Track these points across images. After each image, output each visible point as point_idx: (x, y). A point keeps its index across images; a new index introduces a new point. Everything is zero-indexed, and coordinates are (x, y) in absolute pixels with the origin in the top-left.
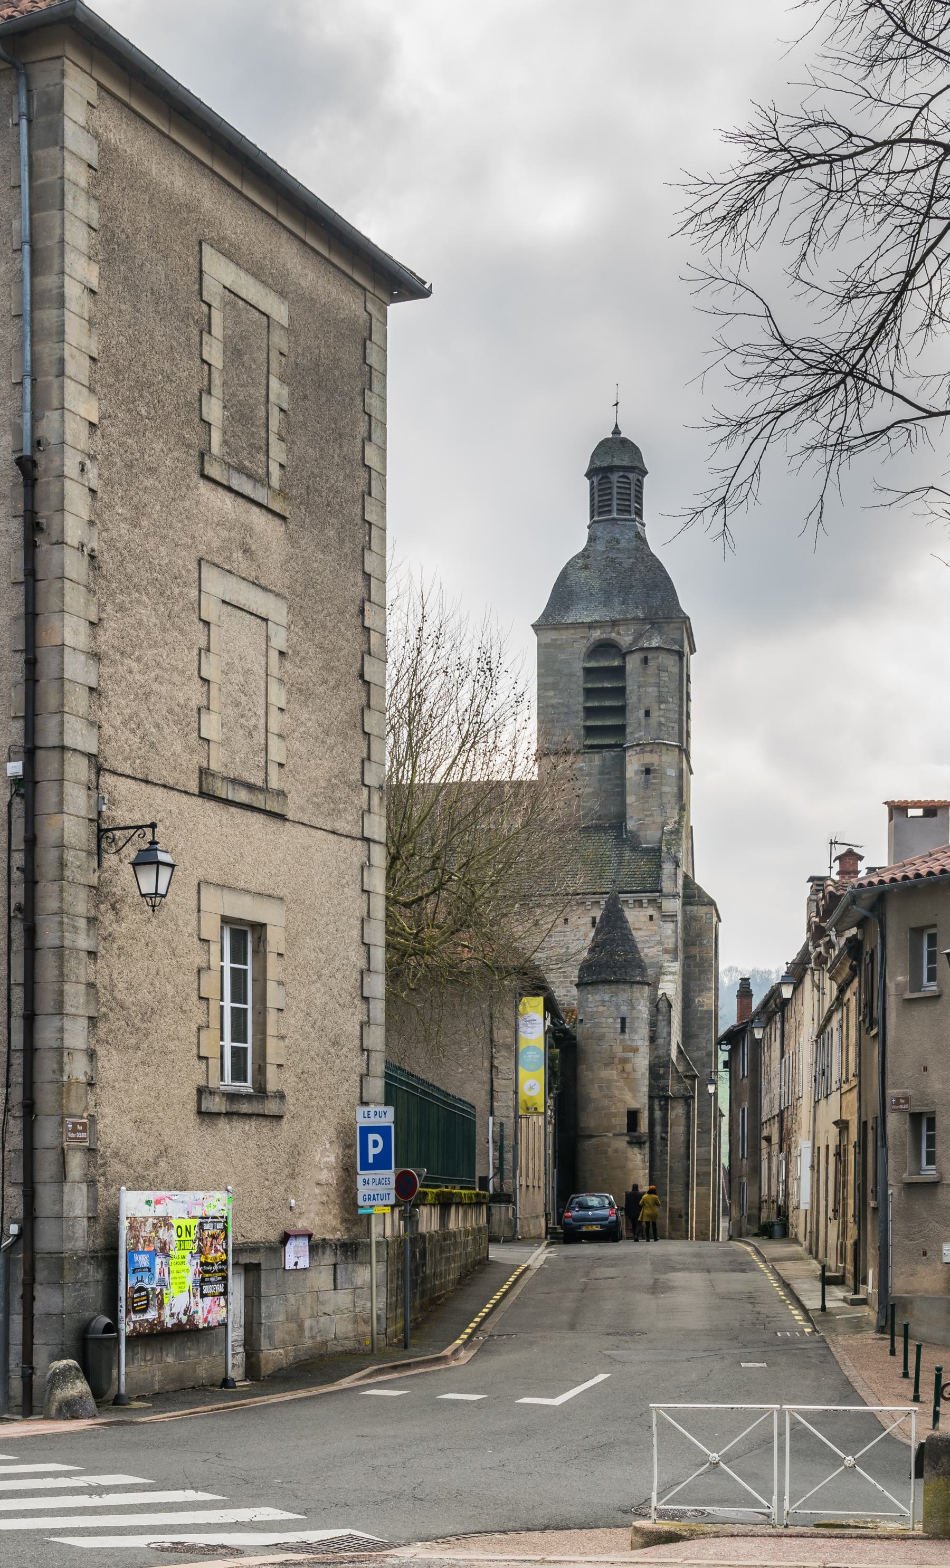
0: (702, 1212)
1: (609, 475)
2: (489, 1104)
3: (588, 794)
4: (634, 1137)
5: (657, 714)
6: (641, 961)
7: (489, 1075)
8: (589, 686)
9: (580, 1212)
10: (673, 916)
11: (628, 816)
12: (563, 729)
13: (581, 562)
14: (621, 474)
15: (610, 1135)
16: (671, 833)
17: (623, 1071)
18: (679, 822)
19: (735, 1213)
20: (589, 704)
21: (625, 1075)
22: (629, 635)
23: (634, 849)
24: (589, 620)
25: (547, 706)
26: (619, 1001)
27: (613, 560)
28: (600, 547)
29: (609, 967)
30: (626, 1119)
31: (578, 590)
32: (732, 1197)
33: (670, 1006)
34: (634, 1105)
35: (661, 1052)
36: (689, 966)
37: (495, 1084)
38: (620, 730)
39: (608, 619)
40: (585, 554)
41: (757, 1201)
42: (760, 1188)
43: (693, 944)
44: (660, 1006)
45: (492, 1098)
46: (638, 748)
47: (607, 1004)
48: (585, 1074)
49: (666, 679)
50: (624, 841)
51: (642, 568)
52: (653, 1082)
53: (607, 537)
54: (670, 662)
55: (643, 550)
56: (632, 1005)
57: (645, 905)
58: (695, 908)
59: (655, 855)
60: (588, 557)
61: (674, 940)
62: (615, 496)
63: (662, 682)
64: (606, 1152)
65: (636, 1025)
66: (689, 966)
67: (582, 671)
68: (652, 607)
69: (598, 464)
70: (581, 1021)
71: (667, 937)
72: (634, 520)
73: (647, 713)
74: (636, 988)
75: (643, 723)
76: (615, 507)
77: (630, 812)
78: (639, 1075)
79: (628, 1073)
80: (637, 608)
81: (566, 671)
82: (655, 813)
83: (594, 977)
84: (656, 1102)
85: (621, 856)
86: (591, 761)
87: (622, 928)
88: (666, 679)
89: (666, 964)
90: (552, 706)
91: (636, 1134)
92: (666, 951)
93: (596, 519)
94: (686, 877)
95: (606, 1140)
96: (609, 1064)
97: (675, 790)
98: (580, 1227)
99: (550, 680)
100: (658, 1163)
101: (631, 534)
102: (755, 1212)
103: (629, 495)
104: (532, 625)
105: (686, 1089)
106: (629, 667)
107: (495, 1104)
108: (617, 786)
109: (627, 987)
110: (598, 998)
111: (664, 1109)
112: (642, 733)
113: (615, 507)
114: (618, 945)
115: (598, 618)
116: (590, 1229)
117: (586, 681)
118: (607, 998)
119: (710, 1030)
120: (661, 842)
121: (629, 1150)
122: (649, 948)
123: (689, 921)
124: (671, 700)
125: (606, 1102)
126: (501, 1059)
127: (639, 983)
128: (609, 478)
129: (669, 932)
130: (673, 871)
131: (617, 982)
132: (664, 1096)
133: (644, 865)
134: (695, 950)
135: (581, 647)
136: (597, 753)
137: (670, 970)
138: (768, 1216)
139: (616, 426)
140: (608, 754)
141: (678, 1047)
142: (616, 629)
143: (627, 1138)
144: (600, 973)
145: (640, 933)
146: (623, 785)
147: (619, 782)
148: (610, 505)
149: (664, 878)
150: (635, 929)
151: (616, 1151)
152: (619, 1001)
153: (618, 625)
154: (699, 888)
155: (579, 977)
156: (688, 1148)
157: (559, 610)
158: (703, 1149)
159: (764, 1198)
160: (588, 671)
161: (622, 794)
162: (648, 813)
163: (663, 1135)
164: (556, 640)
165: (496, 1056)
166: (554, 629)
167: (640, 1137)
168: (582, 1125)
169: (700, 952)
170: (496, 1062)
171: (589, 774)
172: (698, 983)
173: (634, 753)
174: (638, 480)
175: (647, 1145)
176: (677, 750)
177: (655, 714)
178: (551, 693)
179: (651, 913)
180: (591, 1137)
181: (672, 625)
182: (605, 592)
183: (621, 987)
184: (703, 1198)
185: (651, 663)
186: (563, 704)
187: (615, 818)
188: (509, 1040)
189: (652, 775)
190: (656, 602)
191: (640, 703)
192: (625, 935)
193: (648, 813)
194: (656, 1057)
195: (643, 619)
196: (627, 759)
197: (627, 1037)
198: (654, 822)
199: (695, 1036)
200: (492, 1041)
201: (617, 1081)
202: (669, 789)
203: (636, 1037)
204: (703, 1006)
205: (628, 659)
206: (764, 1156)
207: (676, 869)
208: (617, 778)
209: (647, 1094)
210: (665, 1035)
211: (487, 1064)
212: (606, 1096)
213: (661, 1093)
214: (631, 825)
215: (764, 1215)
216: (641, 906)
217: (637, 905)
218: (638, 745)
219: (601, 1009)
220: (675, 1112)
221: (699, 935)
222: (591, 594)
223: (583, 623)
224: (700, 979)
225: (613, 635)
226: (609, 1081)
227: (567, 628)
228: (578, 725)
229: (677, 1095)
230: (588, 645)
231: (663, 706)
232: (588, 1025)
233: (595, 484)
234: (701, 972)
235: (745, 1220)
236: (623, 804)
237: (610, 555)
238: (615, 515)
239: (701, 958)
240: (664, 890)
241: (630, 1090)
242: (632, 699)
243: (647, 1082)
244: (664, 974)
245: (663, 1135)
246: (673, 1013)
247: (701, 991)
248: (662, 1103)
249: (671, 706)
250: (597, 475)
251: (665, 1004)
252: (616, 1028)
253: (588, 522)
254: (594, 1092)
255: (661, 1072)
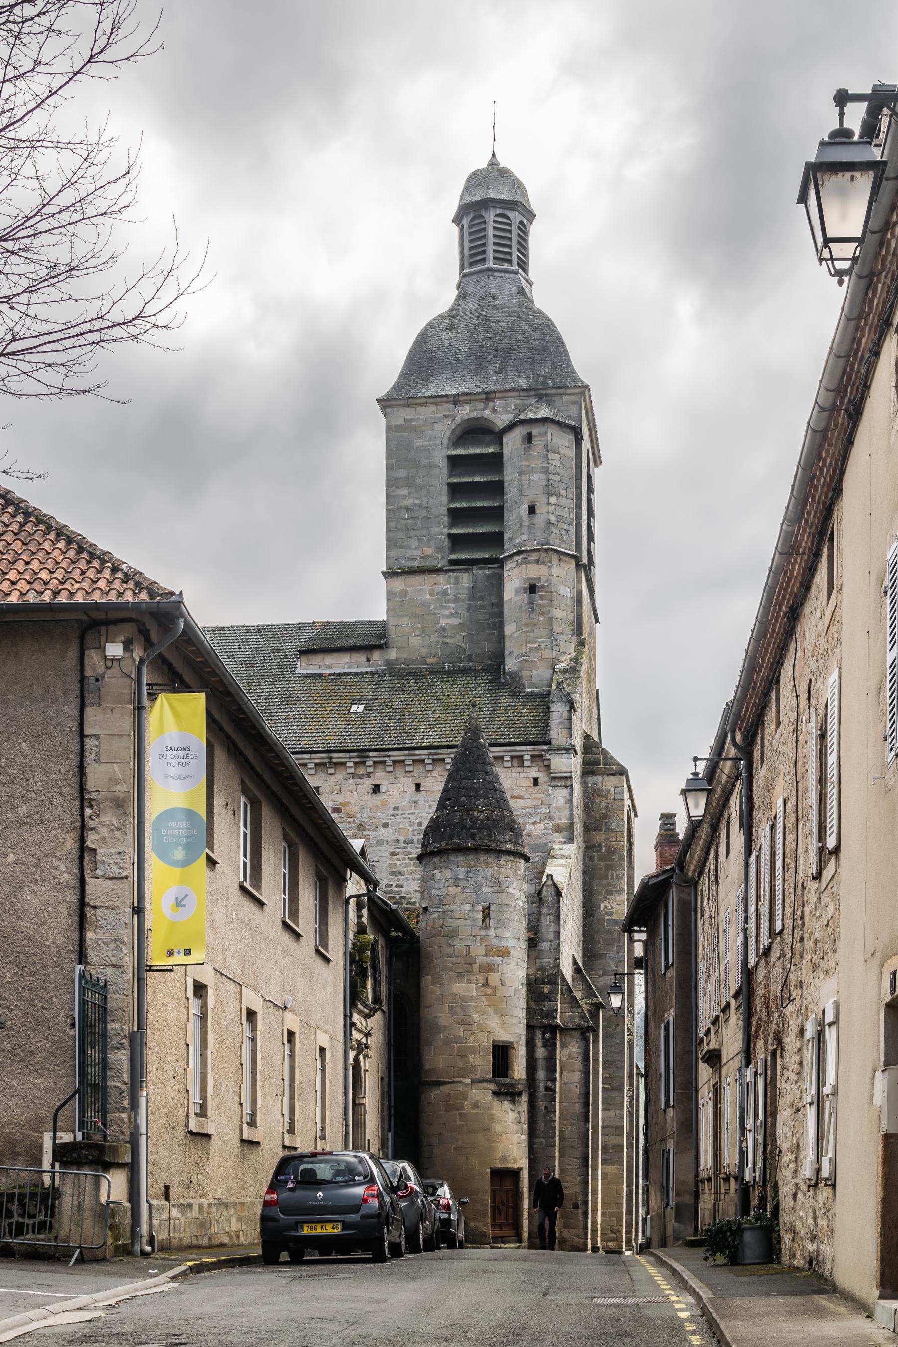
0: (611, 1201)
1: (483, 213)
2: (75, 936)
3: (454, 627)
4: (504, 1085)
5: (545, 510)
6: (514, 821)
7: (76, 870)
8: (455, 480)
9: (299, 1193)
10: (566, 778)
11: (507, 653)
12: (420, 540)
13: (445, 323)
14: (499, 211)
15: (467, 1080)
16: (565, 671)
17: (487, 984)
18: (577, 660)
19: (655, 1202)
20: (454, 505)
21: (489, 991)
22: (508, 412)
23: (514, 695)
24: (454, 392)
25: (399, 509)
26: (480, 878)
27: (487, 319)
28: (471, 304)
29: (464, 827)
30: (491, 1056)
31: (440, 355)
32: (651, 1176)
33: (559, 893)
34: (504, 1036)
35: (546, 961)
36: (591, 858)
37: (89, 889)
38: (497, 540)
39: (480, 390)
40: (452, 314)
41: (691, 1179)
42: (697, 1158)
43: (597, 829)
44: (544, 893)
45: (82, 924)
46: (519, 558)
47: (461, 883)
48: (431, 989)
49: (558, 464)
50: (502, 686)
51: (527, 327)
52: (533, 1004)
53: (481, 293)
54: (562, 440)
55: (528, 307)
56: (499, 886)
57: (527, 763)
58: (599, 779)
59: (543, 700)
60: (455, 316)
61: (567, 812)
62: (491, 240)
63: (551, 468)
64: (460, 1107)
65: (506, 915)
66: (591, 858)
67: (445, 461)
68: (539, 376)
69: (468, 199)
70: (425, 909)
71: (559, 809)
72: (517, 273)
73: (532, 510)
74: (505, 860)
75: (526, 523)
76: (491, 254)
77: (509, 646)
78: (510, 991)
79: (494, 988)
80: (519, 376)
81: (425, 462)
82: (543, 646)
83: (443, 843)
84: (539, 1034)
85: (495, 703)
86: (457, 580)
87: (485, 771)
88: (558, 464)
89: (556, 846)
90: (406, 508)
91: (508, 1080)
92: (557, 829)
93: (467, 271)
94: (587, 737)
95: (461, 1088)
96: (463, 974)
97: (571, 616)
98: (297, 1225)
99: (402, 473)
100: (541, 1126)
101: (514, 290)
102: (689, 1199)
103: (510, 239)
104: (378, 400)
105: (583, 1017)
106: (507, 450)
107: (90, 936)
108: (493, 615)
109: (492, 859)
110: (448, 874)
111: (550, 1045)
112: (525, 537)
113: (491, 254)
114: (478, 797)
115: (466, 390)
116: (319, 1231)
117: (451, 475)
118: (461, 873)
119: (621, 947)
120: (551, 686)
121: (496, 1104)
122: (532, 824)
123: (591, 797)
124: (564, 493)
125: (461, 1031)
126: (104, 831)
127: (509, 853)
128: (483, 216)
129: (561, 802)
130: (566, 714)
131: (476, 850)
132: (550, 1025)
133: (527, 713)
134: (599, 837)
135: (444, 430)
136: (466, 570)
137: (562, 852)
138: (715, 1209)
139: (494, 155)
140: (481, 572)
141: (575, 963)
142: (491, 404)
143: (493, 1087)
144: (451, 837)
145: (521, 803)
146: (501, 614)
147: (495, 609)
148: (484, 252)
149: (553, 724)
150: (513, 797)
151: (476, 1105)
152: (480, 878)
153: (493, 399)
154: (605, 753)
155: (423, 846)
156: (586, 1104)
157: (415, 382)
158: (612, 1113)
159: (704, 1175)
160: (454, 462)
161: (500, 626)
162: (533, 646)
163: (549, 1084)
164: (411, 420)
165: (91, 824)
166: (408, 405)
167: (513, 1085)
168: (427, 1066)
169: (606, 839)
170: (91, 840)
171: (456, 600)
172: (604, 881)
173: (514, 564)
174: (521, 222)
175: (525, 1097)
176: (573, 562)
177: (540, 510)
178: (404, 492)
179: (537, 775)
180: (439, 1083)
181: (566, 399)
182: (477, 357)
183: (483, 857)
184: (611, 1181)
185: (536, 441)
186: (420, 506)
187: (490, 659)
188: (123, 789)
189: (538, 594)
190: (544, 370)
191: (521, 495)
192: (490, 782)
193: (533, 646)
194: (539, 969)
195: (527, 390)
196: (506, 574)
197: (491, 932)
198: (541, 658)
199: (602, 956)
200: (82, 789)
201: (477, 999)
202: (563, 614)
203: (506, 934)
204: (611, 914)
205: (506, 438)
206: (705, 1095)
207: (570, 711)
208: (492, 604)
209: (524, 1021)
210: (551, 936)
211: (71, 843)
212: (460, 1022)
213: (545, 1021)
214: (511, 664)
215: (706, 1203)
216: (522, 765)
217: (516, 763)
218: (520, 553)
219: (453, 890)
220: (566, 1051)
221: (605, 816)
222: (458, 360)
223: (446, 396)
224: (606, 877)
225: (487, 413)
226: (465, 1000)
227: (426, 404)
228: (441, 534)
229: (570, 1025)
230: (454, 426)
231: (553, 500)
232: (435, 916)
233: (466, 226)
234: (608, 868)
235: (671, 1214)
236: (501, 638)
237: (484, 313)
238: (491, 264)
239: (608, 848)
240: (554, 742)
241: (498, 1013)
242: (511, 493)
243: (523, 1003)
244: (553, 857)
245: (549, 1084)
246: (564, 908)
247: (608, 893)
248: (547, 1036)
249: (564, 501)
250: (468, 214)
251: (552, 890)
252: (475, 920)
253: (456, 278)
254: (443, 1016)
255: (546, 990)
